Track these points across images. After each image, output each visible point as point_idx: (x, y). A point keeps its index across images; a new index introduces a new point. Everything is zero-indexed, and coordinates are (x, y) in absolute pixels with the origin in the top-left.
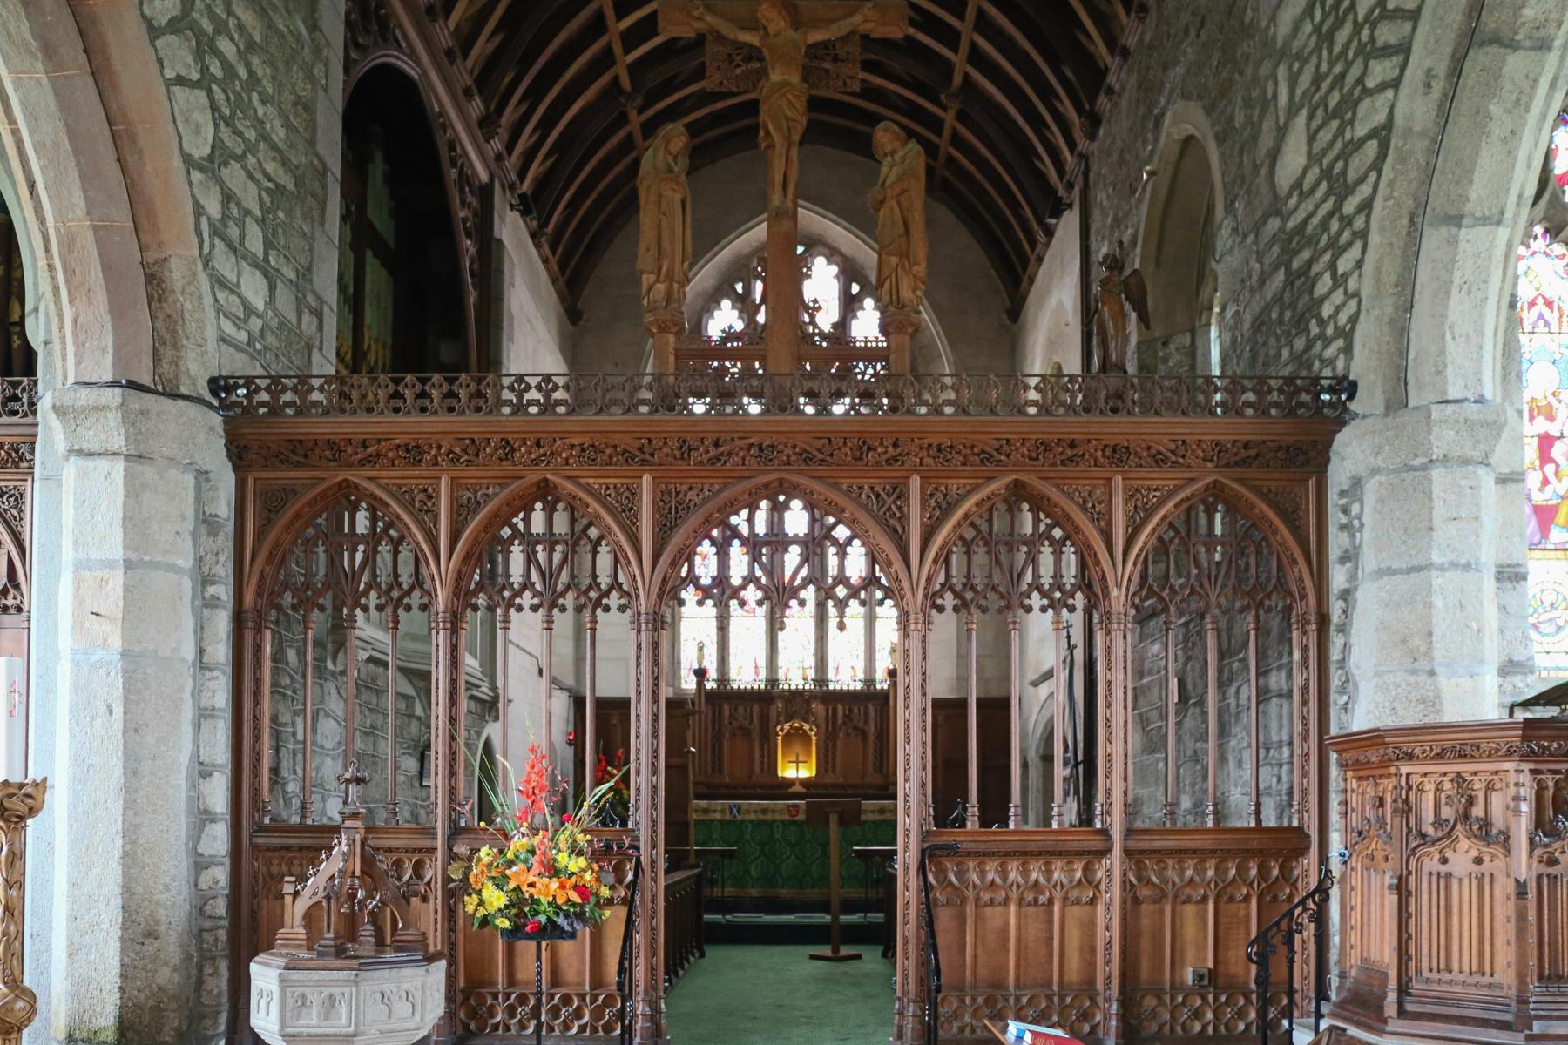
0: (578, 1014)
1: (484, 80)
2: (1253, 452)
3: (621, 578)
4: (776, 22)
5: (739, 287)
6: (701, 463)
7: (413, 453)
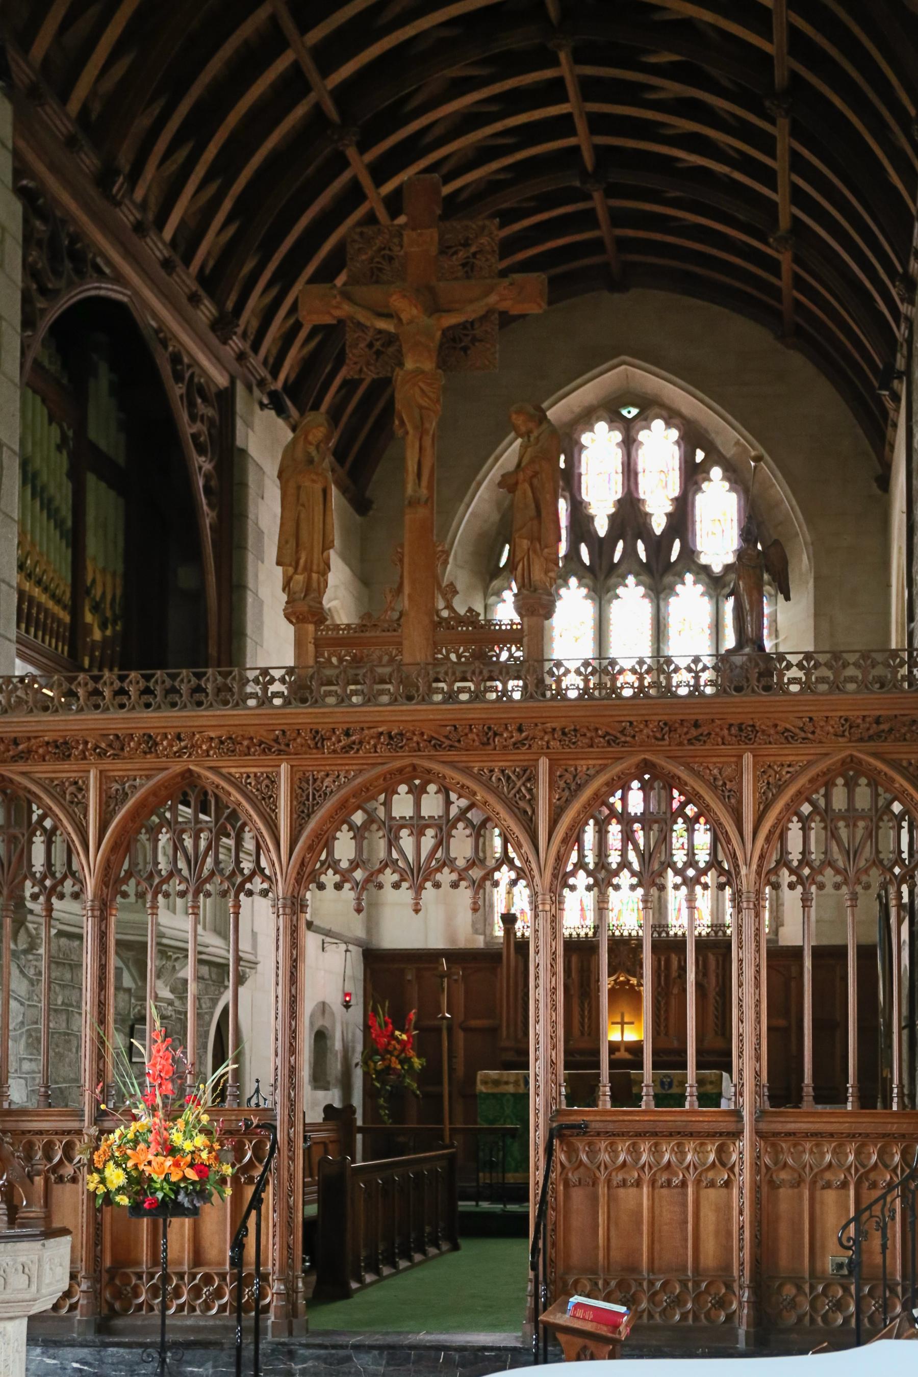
0: (219, 1294)
1: (211, 282)
2: (885, 727)
3: (264, 863)
4: (409, 310)
6: (334, 751)
7: (62, 749)
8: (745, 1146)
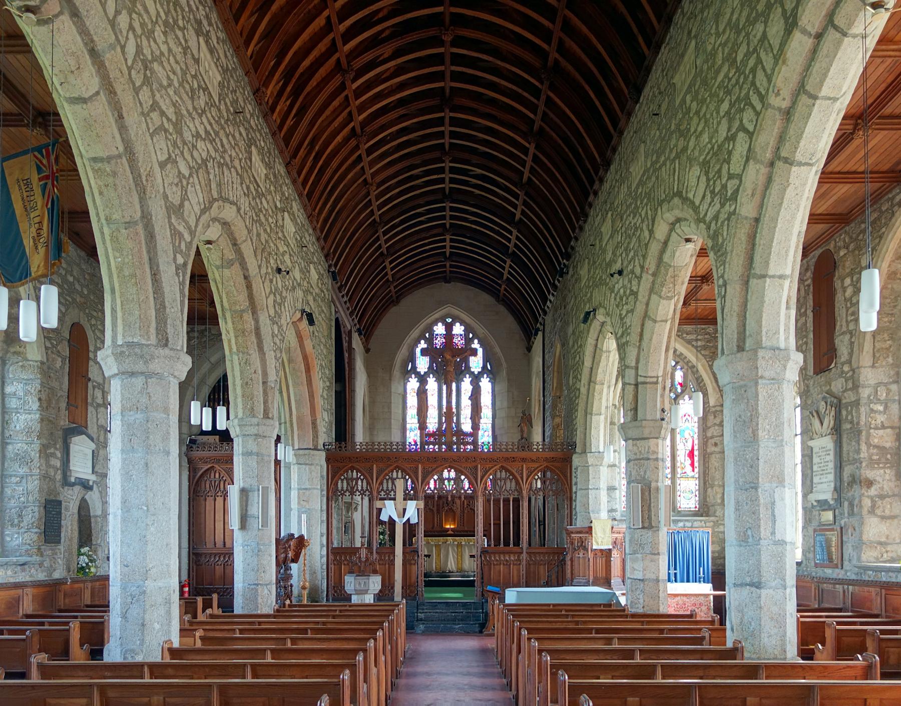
5: (427, 335)
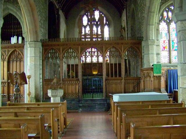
5: (87, 14)
8: (123, 80)
